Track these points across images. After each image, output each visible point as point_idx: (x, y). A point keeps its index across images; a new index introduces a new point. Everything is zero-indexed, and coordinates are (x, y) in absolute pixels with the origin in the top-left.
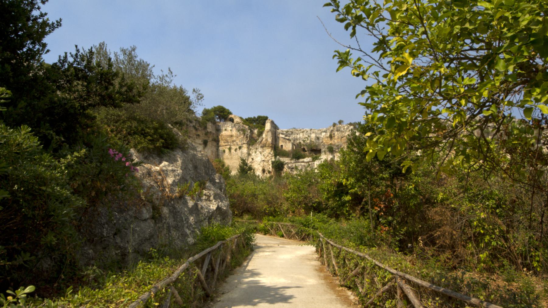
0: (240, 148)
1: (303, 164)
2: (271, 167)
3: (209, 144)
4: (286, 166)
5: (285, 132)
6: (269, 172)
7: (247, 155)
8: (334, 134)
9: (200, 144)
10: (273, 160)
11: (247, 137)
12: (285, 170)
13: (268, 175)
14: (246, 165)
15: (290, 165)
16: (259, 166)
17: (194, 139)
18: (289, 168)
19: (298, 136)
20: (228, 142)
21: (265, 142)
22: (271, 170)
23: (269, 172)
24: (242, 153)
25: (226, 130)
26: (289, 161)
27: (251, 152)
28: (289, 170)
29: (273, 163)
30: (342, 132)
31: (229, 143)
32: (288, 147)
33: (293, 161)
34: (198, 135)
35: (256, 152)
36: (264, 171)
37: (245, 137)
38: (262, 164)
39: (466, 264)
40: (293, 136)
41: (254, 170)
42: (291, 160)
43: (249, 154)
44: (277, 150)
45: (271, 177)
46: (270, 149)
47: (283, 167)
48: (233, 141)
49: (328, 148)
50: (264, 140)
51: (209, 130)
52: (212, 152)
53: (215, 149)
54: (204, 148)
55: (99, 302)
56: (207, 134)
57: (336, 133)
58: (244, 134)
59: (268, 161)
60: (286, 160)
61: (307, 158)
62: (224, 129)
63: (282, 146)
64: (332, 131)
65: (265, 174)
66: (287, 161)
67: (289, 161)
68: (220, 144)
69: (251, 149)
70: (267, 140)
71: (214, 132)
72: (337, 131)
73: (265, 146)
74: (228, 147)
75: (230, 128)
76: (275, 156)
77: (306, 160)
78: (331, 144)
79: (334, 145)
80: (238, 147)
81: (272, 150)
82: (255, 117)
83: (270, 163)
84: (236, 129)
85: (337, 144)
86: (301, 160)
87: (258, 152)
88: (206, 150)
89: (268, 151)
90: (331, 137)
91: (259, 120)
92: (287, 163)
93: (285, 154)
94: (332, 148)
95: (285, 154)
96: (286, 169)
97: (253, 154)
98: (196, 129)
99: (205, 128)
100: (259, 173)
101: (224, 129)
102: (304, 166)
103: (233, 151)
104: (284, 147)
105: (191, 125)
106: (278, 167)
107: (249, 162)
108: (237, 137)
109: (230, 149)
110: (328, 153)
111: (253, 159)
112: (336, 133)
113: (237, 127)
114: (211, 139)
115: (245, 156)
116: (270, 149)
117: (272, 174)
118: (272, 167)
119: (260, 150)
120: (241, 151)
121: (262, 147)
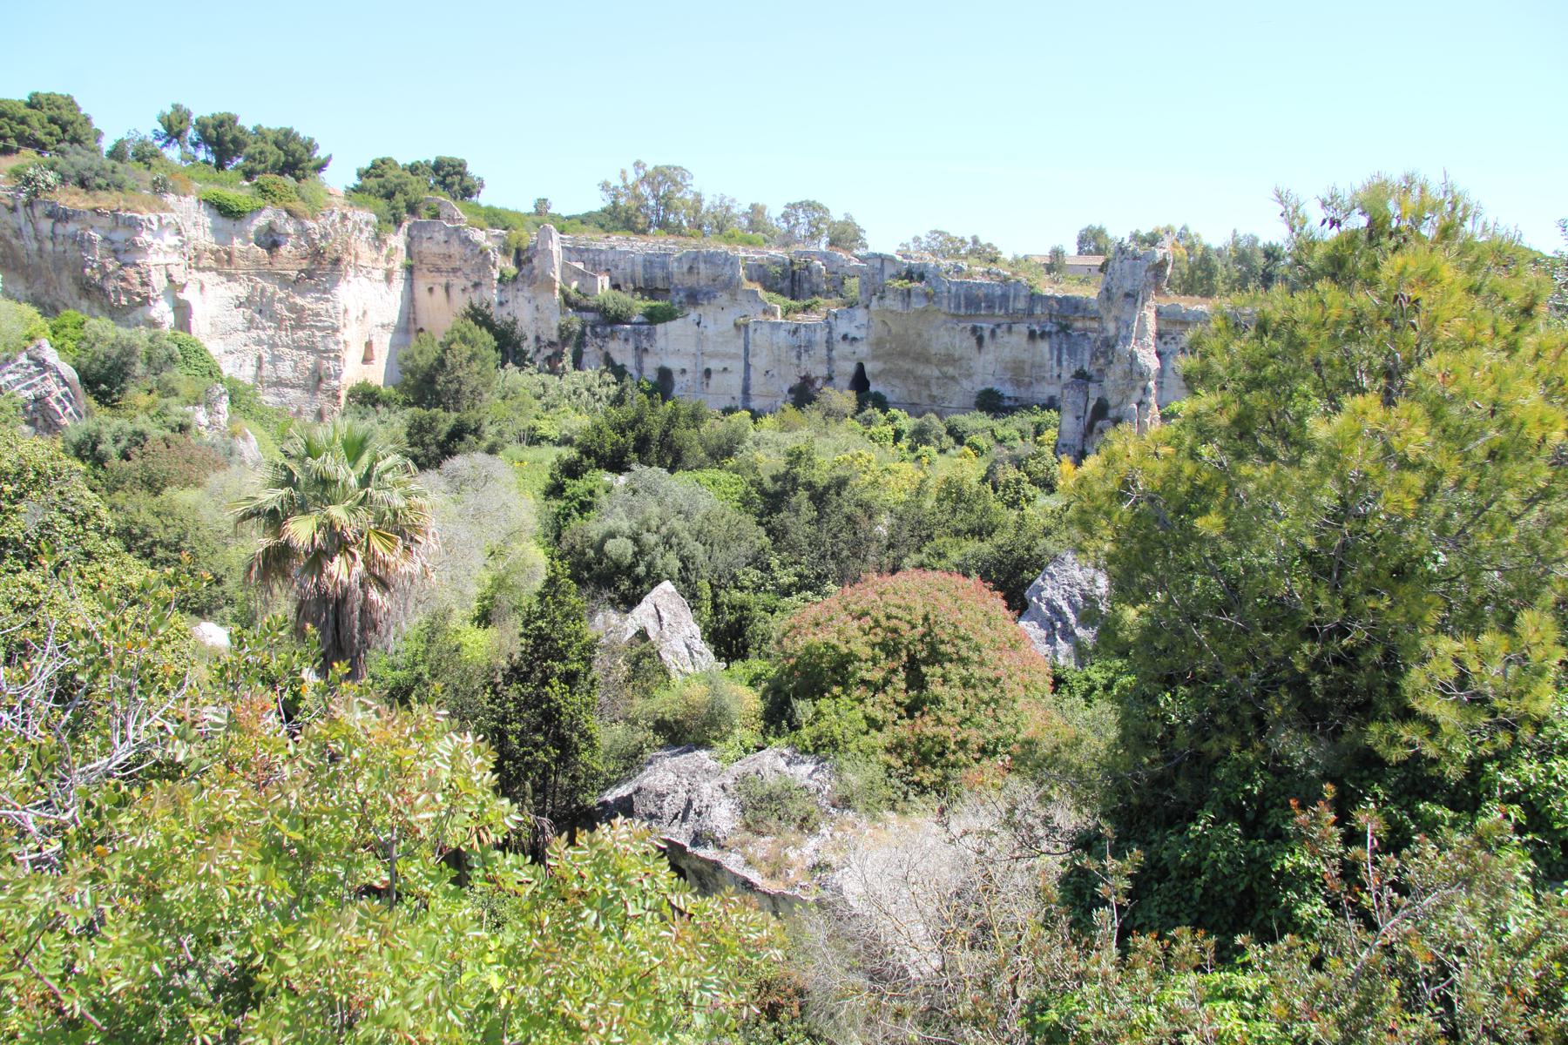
57: (702, 266)
80: (469, 284)
109: (447, 288)
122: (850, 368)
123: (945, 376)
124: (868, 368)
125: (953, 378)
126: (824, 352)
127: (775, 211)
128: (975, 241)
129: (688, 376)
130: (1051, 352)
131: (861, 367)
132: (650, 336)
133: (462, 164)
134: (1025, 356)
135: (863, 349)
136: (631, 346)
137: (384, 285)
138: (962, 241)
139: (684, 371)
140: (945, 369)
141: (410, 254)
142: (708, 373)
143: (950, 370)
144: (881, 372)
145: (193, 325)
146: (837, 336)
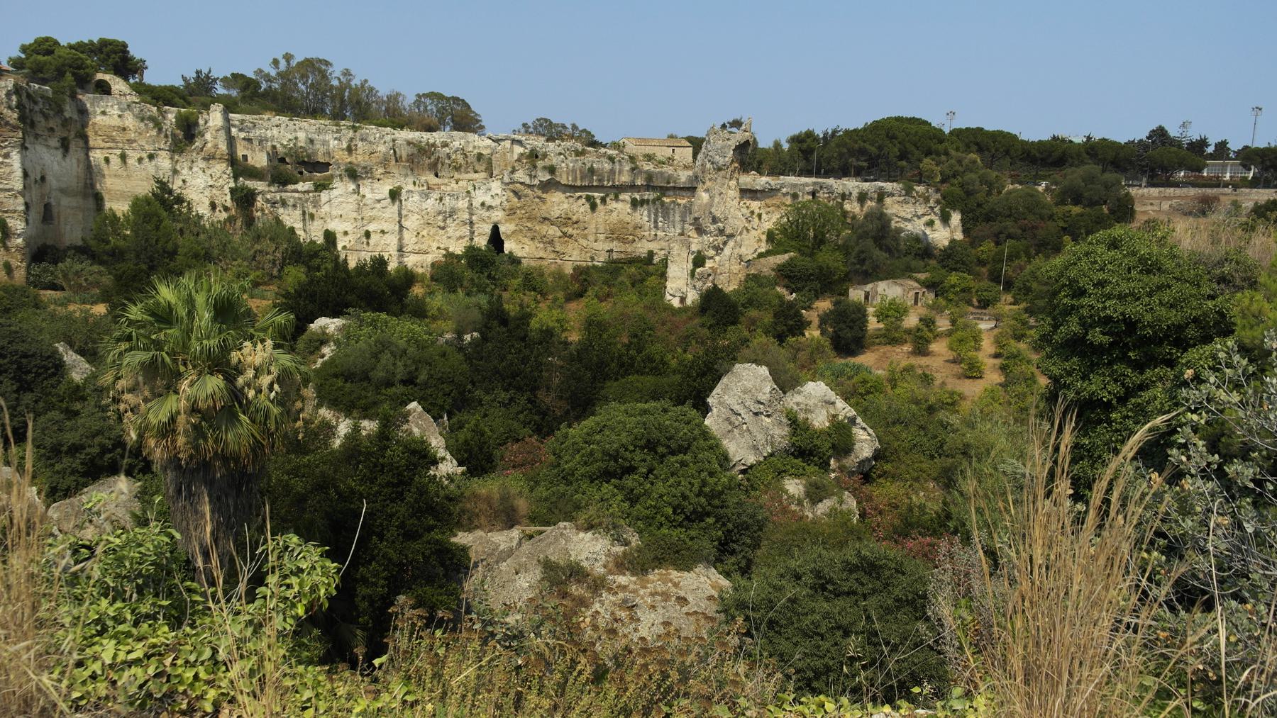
0: (151, 157)
1: (296, 195)
2: (228, 197)
3: (72, 147)
4: (259, 198)
5: (237, 123)
6: (226, 209)
7: (170, 173)
8: (356, 145)
9: (56, 148)
10: (232, 185)
11: (166, 136)
12: (258, 205)
13: (224, 215)
14: (170, 192)
15: (269, 197)
16: (201, 195)
17: (46, 140)
18: (268, 201)
19: (269, 134)
20: (114, 141)
21: (213, 150)
22: (229, 204)
23: (226, 209)
24: (157, 168)
25: (104, 113)
26: (267, 189)
27: (178, 168)
28: (267, 207)
29: (232, 191)
30: (370, 142)
31: (120, 145)
32: (259, 160)
33: (273, 189)
34: (52, 129)
35: (191, 168)
36: (213, 206)
37: (162, 135)
38: (207, 193)
39: (113, 56)
40: (258, 133)
41: (189, 203)
42: (269, 186)
43: (175, 172)
44: (239, 168)
45: (231, 220)
46: (224, 165)
47: (254, 200)
48: (130, 141)
49: (346, 170)
50: (209, 145)
51: (67, 115)
52: (78, 160)
53: (82, 156)
54: (64, 156)
55: (502, 348)
56: (66, 123)
57: (360, 144)
58: (160, 130)
59: (223, 187)
60: (259, 186)
61: (301, 184)
62: (99, 111)
63: (245, 157)
64: (352, 139)
65: (217, 213)
66: (260, 189)
67: (267, 189)
68: (91, 143)
69: (177, 161)
70: (216, 146)
71: (75, 117)
72: (362, 140)
73: (214, 158)
74: (118, 152)
75: (115, 111)
76: (236, 178)
77: (301, 186)
78: (350, 163)
79: (358, 165)
80: (145, 155)
81: (228, 166)
82: (91, 43)
83: (227, 191)
84: (136, 116)
85: (363, 164)
86: (291, 187)
87: (195, 169)
88: (68, 159)
89: (220, 168)
90: (349, 150)
91: (105, 50)
92: (262, 193)
93: (254, 174)
94: (355, 171)
95: (254, 174)
96: (260, 203)
97: (185, 172)
98: (46, 117)
99: (60, 111)
100: (203, 209)
101: (99, 111)
102: (300, 199)
103: (132, 161)
104: (249, 159)
105: (37, 108)
106: (244, 199)
107: (176, 186)
108: (140, 134)
109: (123, 157)
110: (346, 179)
111: (184, 181)
112: (360, 144)
113: (136, 111)
114: (72, 134)
115: (165, 173)
116: (224, 165)
117: (233, 212)
118: (232, 199)
119: (202, 164)
120: (153, 163)
121: (207, 159)
122: (487, 229)
123: (565, 234)
124: (502, 229)
125: (571, 236)
126: (466, 216)
127: (409, 99)
128: (574, 127)
129: (350, 237)
130: (649, 216)
131: (495, 229)
132: (316, 204)
133: (125, 45)
134: (628, 219)
135: (498, 215)
136: (298, 213)
137: (59, 153)
138: (564, 126)
139: (346, 233)
140: (565, 230)
141: (314, 113)
142: (368, 235)
143: (570, 231)
144: (514, 232)
145: (699, 136)
146: (476, 203)
